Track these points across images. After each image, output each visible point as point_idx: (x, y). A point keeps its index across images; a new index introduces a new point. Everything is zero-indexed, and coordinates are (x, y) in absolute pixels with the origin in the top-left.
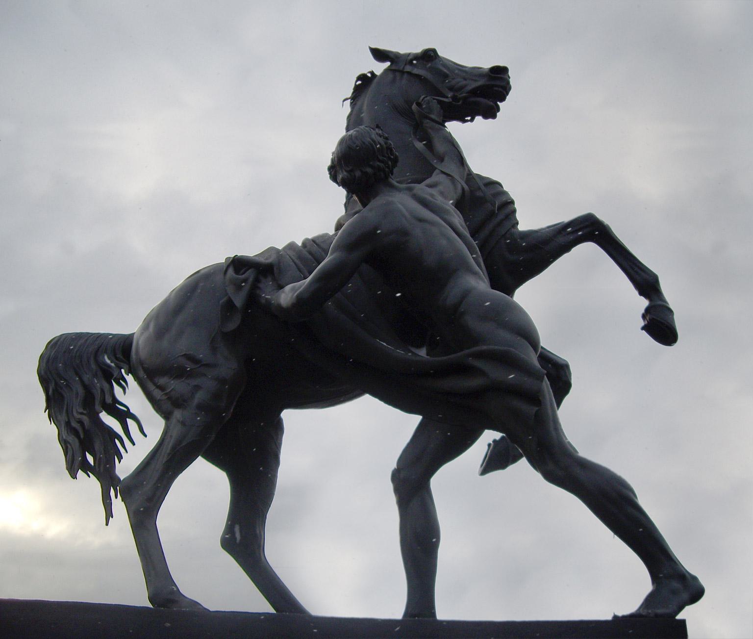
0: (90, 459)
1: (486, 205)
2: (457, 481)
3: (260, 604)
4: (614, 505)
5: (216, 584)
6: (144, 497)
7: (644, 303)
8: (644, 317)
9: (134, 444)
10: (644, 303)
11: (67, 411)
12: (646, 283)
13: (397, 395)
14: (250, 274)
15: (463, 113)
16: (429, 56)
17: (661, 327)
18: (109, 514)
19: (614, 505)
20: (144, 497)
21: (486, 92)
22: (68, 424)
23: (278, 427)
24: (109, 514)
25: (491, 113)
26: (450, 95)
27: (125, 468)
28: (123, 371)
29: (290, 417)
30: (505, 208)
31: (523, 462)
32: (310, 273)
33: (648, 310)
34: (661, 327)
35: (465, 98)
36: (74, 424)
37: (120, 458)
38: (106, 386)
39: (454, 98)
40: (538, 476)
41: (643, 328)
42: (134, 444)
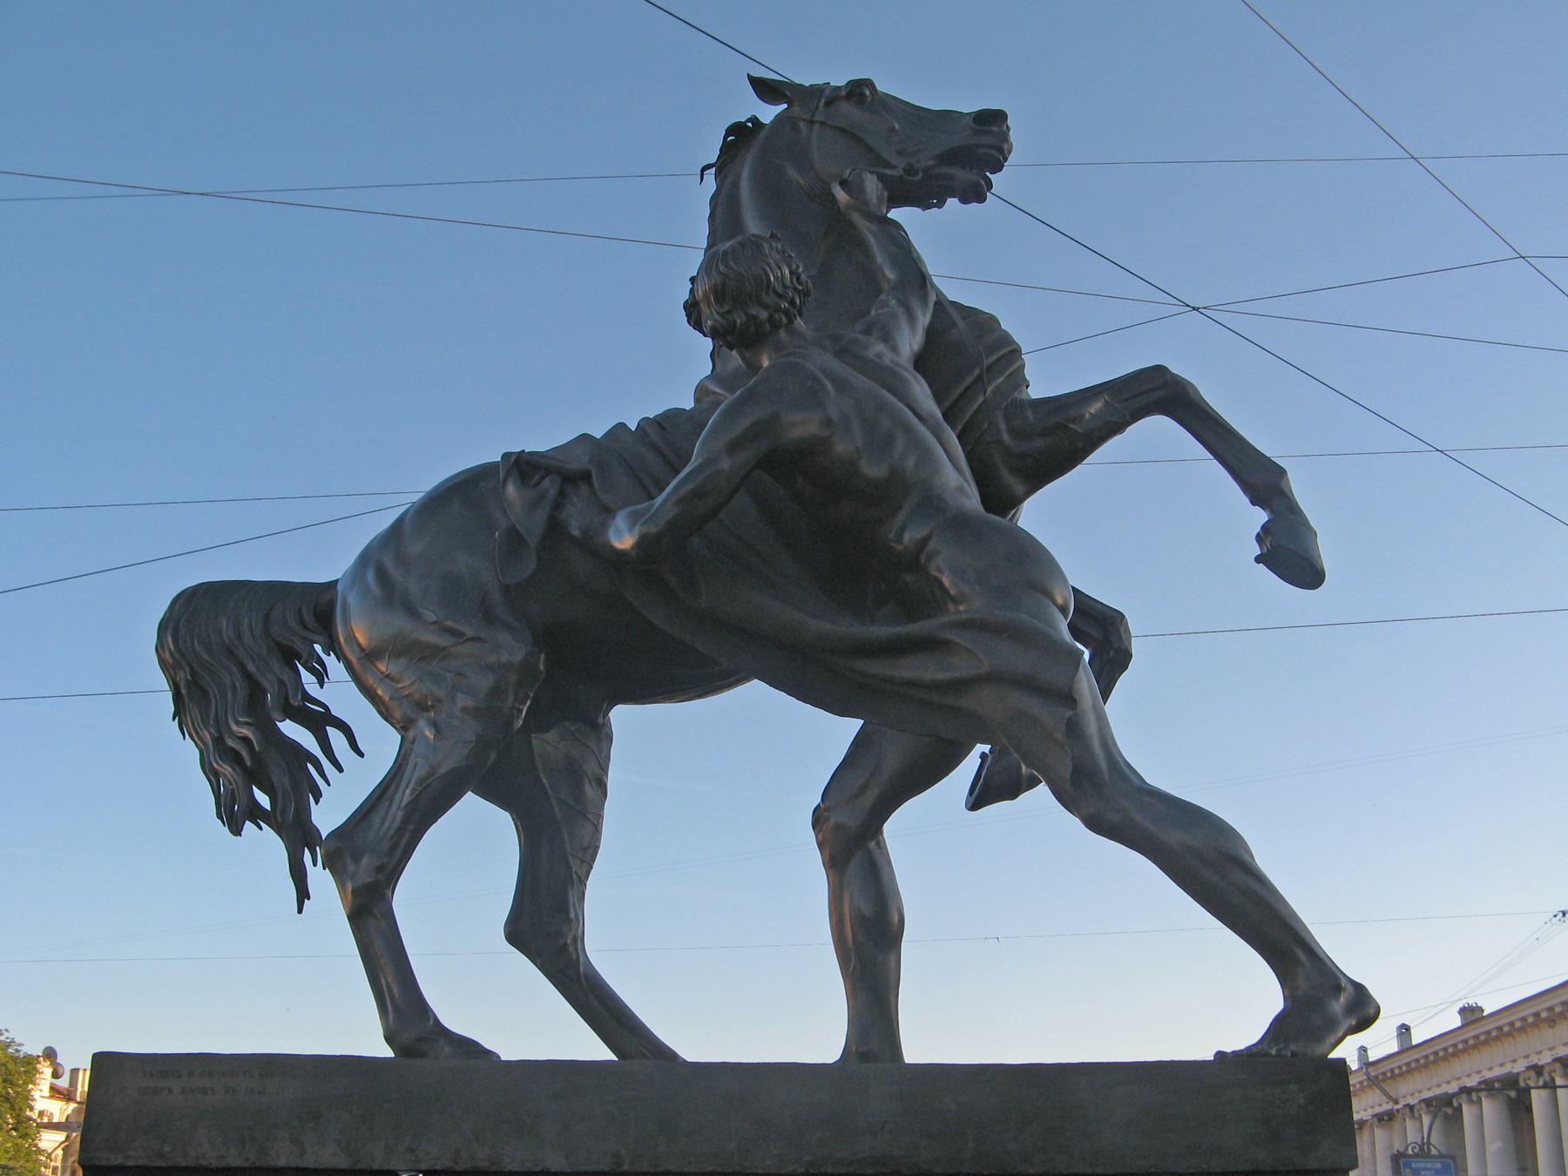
0: (263, 800)
1: (968, 354)
2: (927, 835)
3: (586, 1045)
4: (1214, 870)
5: (516, 1018)
6: (369, 867)
7: (1260, 516)
8: (1259, 539)
9: (340, 770)
10: (1260, 516)
11: (217, 720)
12: (1261, 480)
13: (813, 676)
14: (550, 485)
15: (926, 195)
16: (859, 91)
17: (1290, 555)
18: (303, 894)
19: (1214, 870)
20: (369, 867)
21: (964, 155)
22: (219, 741)
23: (603, 736)
24: (303, 894)
25: (975, 193)
26: (900, 162)
27: (328, 815)
28: (318, 648)
29: (622, 716)
30: (1006, 356)
31: (1042, 791)
32: (662, 490)
33: (1265, 528)
34: (1290, 555)
35: (926, 170)
36: (230, 743)
37: (318, 796)
38: (286, 676)
39: (910, 171)
40: (1075, 823)
41: (1258, 560)
42: (340, 770)
